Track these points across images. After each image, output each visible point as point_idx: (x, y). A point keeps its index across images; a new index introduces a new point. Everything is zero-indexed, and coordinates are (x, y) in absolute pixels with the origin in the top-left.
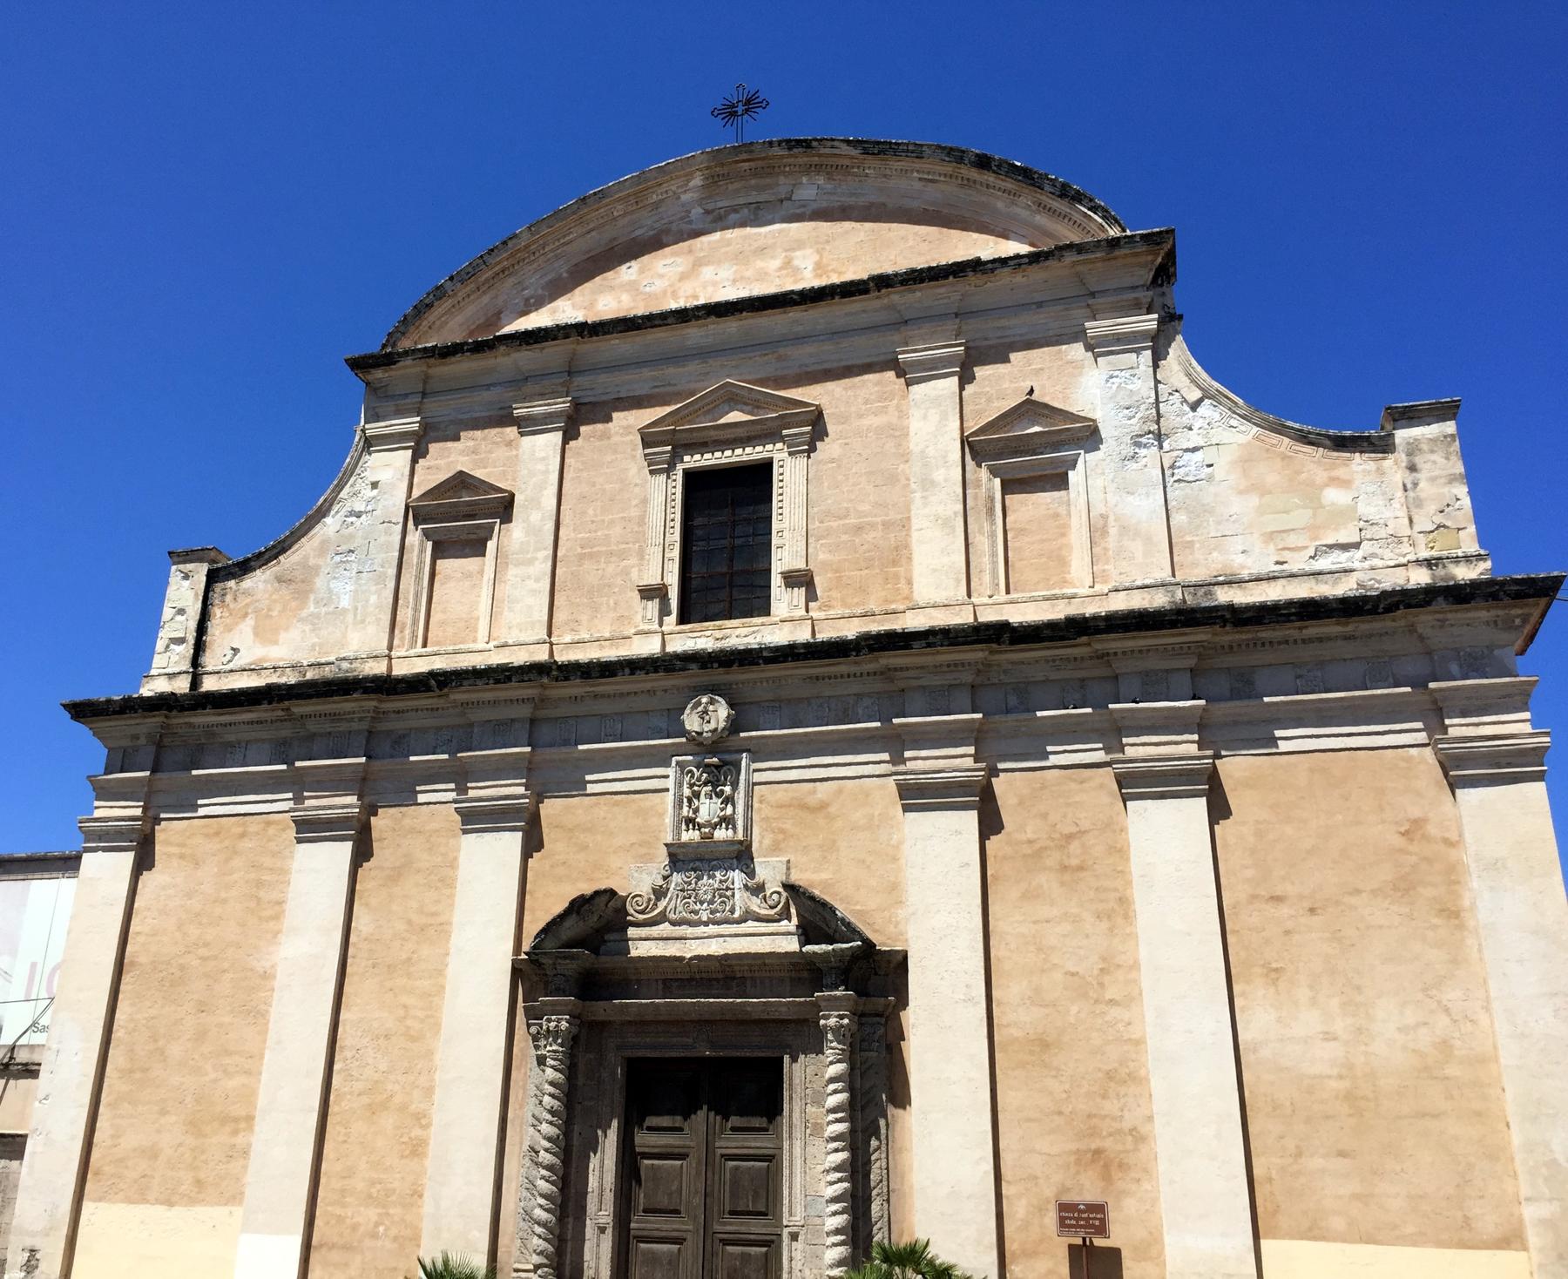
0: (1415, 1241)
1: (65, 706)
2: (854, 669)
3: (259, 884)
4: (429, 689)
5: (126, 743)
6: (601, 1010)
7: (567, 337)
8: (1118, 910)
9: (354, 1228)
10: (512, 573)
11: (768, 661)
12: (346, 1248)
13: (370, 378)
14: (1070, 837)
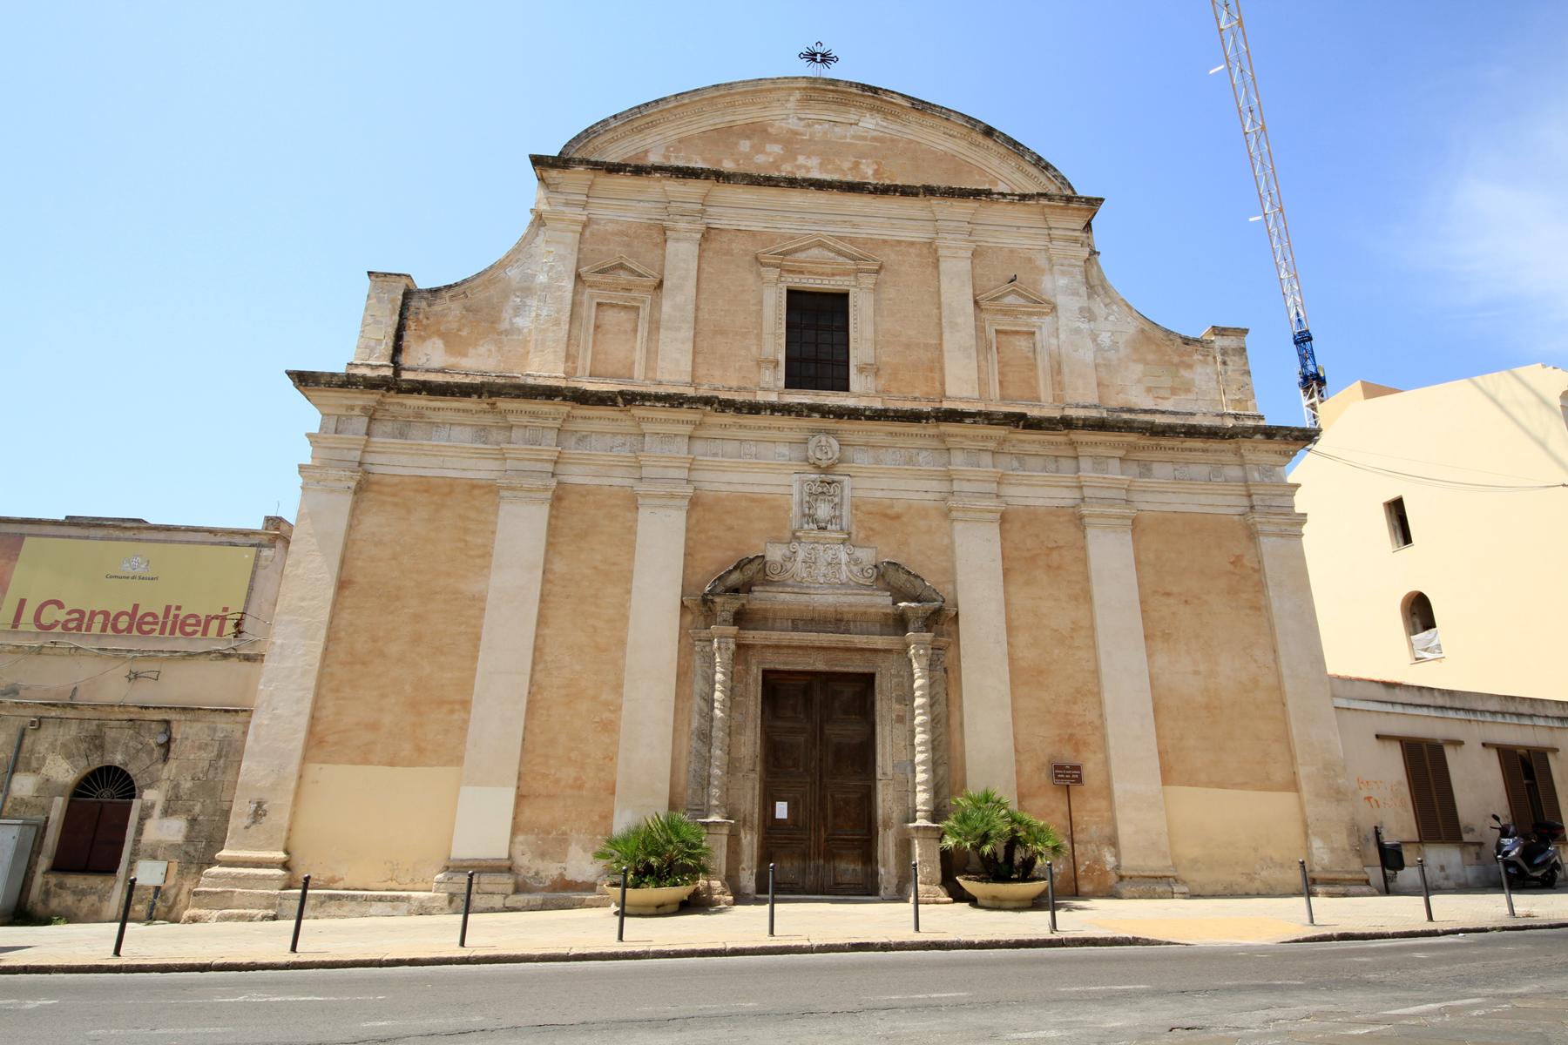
0: (1242, 786)
1: (289, 373)
2: (922, 432)
3: (466, 530)
4: (615, 404)
5: (343, 411)
6: (753, 636)
7: (707, 178)
8: (1084, 596)
9: (558, 781)
10: (664, 335)
11: (869, 418)
12: (550, 797)
13: (545, 175)
14: (1052, 549)
